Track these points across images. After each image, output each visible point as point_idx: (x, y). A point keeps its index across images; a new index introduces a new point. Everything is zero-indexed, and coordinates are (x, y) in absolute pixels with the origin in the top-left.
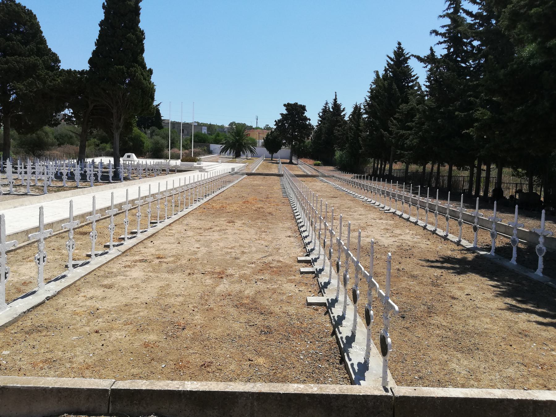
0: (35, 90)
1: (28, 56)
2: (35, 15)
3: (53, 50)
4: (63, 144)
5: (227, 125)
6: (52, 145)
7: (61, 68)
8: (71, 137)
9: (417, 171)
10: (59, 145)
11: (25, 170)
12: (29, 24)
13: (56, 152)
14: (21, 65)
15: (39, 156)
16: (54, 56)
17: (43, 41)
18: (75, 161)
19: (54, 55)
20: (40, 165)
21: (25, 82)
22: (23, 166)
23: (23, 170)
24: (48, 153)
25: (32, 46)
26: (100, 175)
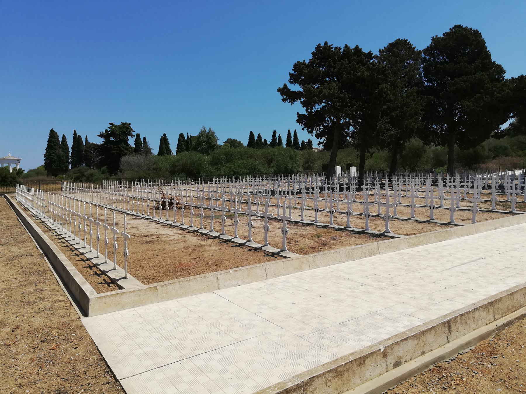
0: (482, 104)
1: (474, 74)
2: (480, 34)
3: (498, 62)
4: (497, 156)
5: (487, 50)
6: (488, 158)
7: (505, 78)
8: (506, 148)
9: (476, 164)
10: (494, 158)
11: (454, 184)
12: (475, 43)
13: (491, 164)
14: (467, 84)
15: (476, 170)
16: (498, 68)
17: (488, 56)
18: (98, 159)
19: (499, 66)
20: (480, 178)
21: (473, 99)
22: (452, 180)
23: (453, 184)
24: (483, 166)
25: (478, 63)
26: (306, 191)
